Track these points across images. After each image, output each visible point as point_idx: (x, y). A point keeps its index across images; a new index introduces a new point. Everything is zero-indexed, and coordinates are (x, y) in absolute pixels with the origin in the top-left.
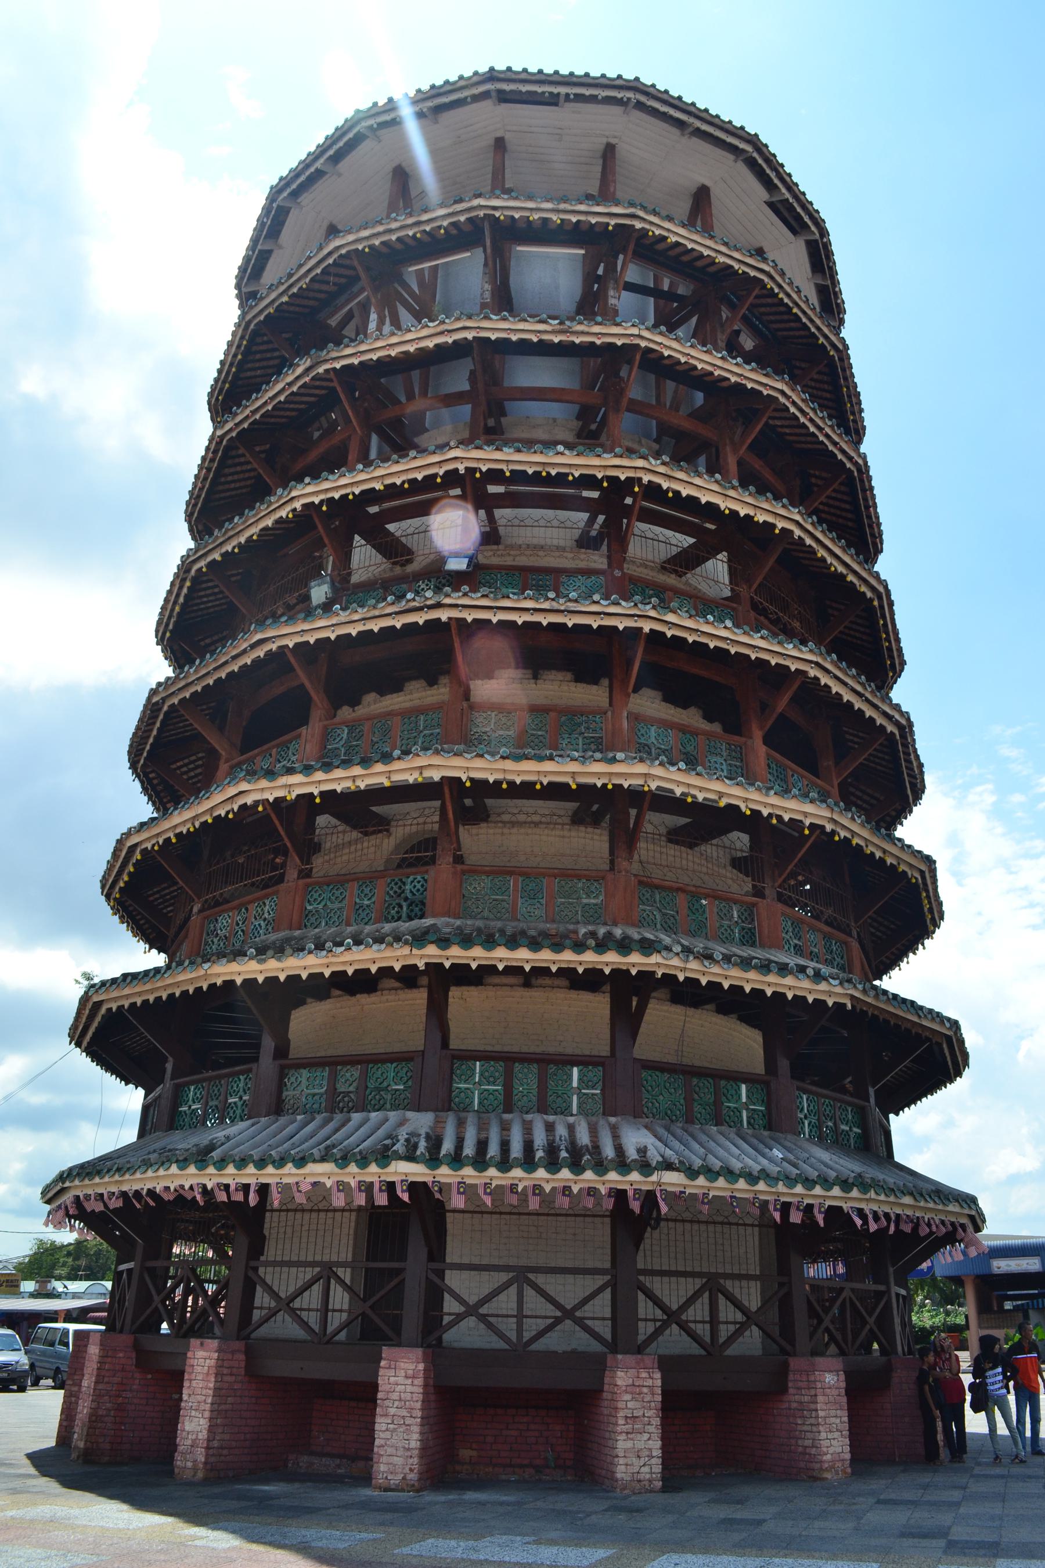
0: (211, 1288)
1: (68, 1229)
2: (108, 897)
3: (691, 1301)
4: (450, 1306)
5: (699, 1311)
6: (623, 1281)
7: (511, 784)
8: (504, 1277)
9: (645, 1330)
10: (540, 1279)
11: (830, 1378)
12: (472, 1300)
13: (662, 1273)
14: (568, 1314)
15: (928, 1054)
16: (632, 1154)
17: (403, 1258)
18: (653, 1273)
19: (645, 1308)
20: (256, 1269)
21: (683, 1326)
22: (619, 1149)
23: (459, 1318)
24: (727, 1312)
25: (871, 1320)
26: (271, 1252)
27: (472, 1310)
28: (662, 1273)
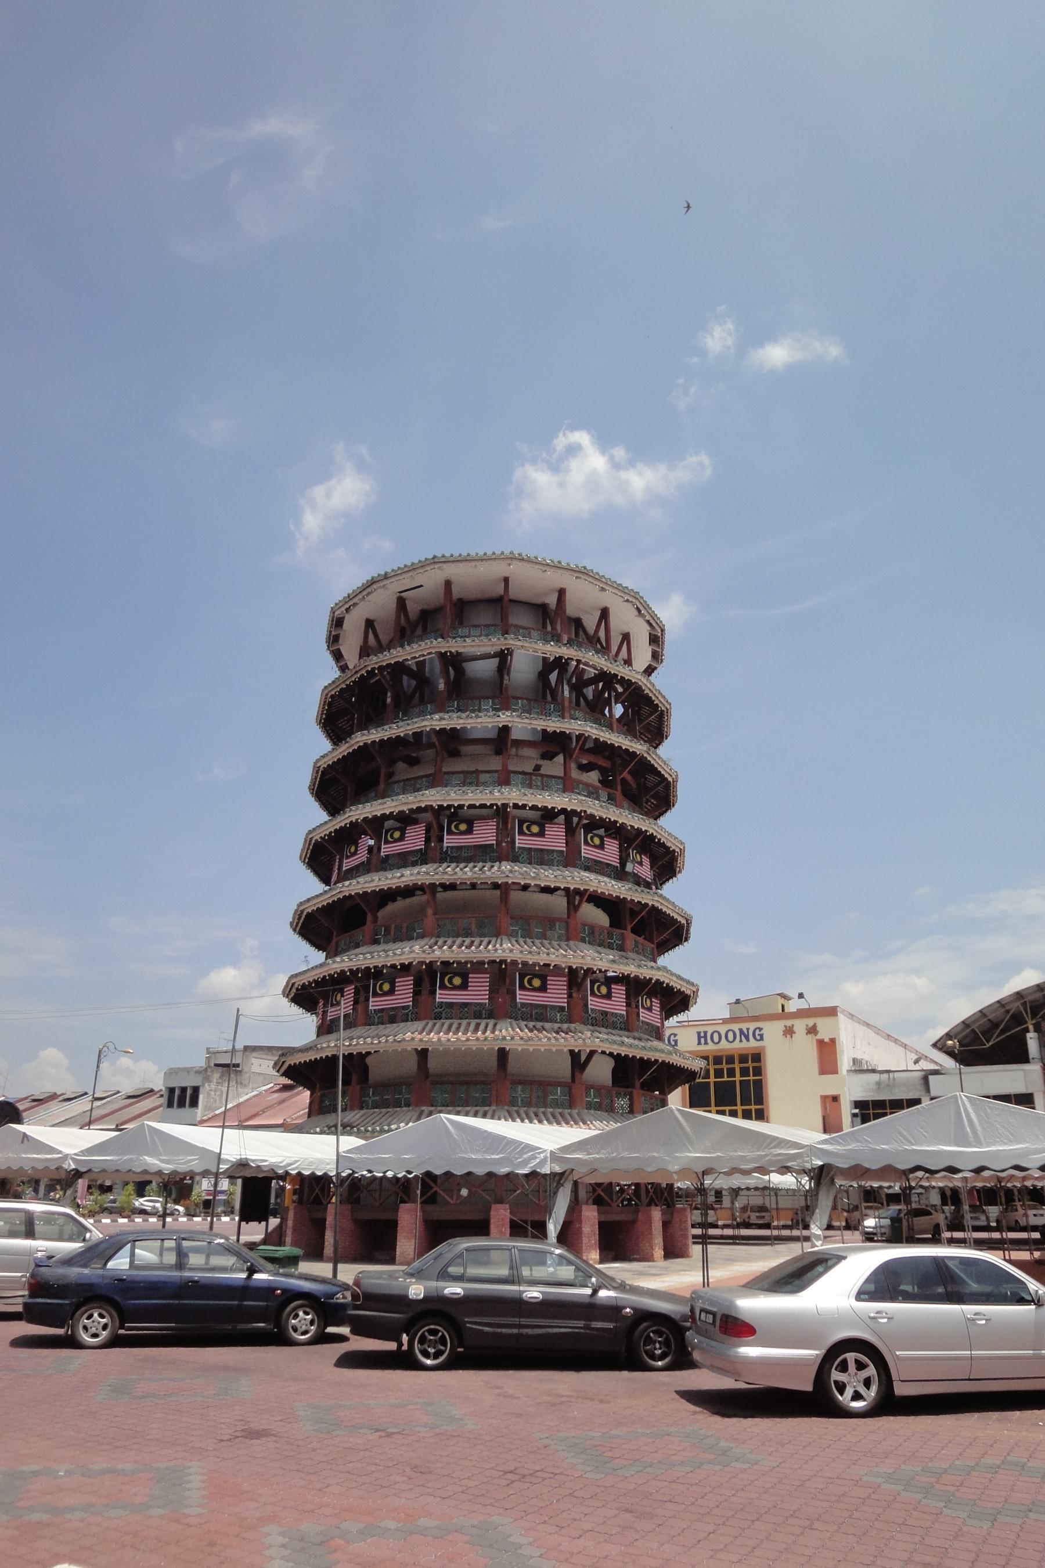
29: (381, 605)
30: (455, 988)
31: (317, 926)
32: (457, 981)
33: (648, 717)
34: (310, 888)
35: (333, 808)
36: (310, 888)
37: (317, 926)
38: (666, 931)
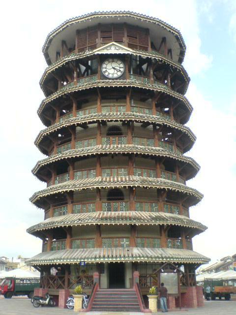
31: (44, 172)
33: (180, 81)
34: (40, 157)
35: (47, 123)
37: (44, 172)
38: (189, 170)
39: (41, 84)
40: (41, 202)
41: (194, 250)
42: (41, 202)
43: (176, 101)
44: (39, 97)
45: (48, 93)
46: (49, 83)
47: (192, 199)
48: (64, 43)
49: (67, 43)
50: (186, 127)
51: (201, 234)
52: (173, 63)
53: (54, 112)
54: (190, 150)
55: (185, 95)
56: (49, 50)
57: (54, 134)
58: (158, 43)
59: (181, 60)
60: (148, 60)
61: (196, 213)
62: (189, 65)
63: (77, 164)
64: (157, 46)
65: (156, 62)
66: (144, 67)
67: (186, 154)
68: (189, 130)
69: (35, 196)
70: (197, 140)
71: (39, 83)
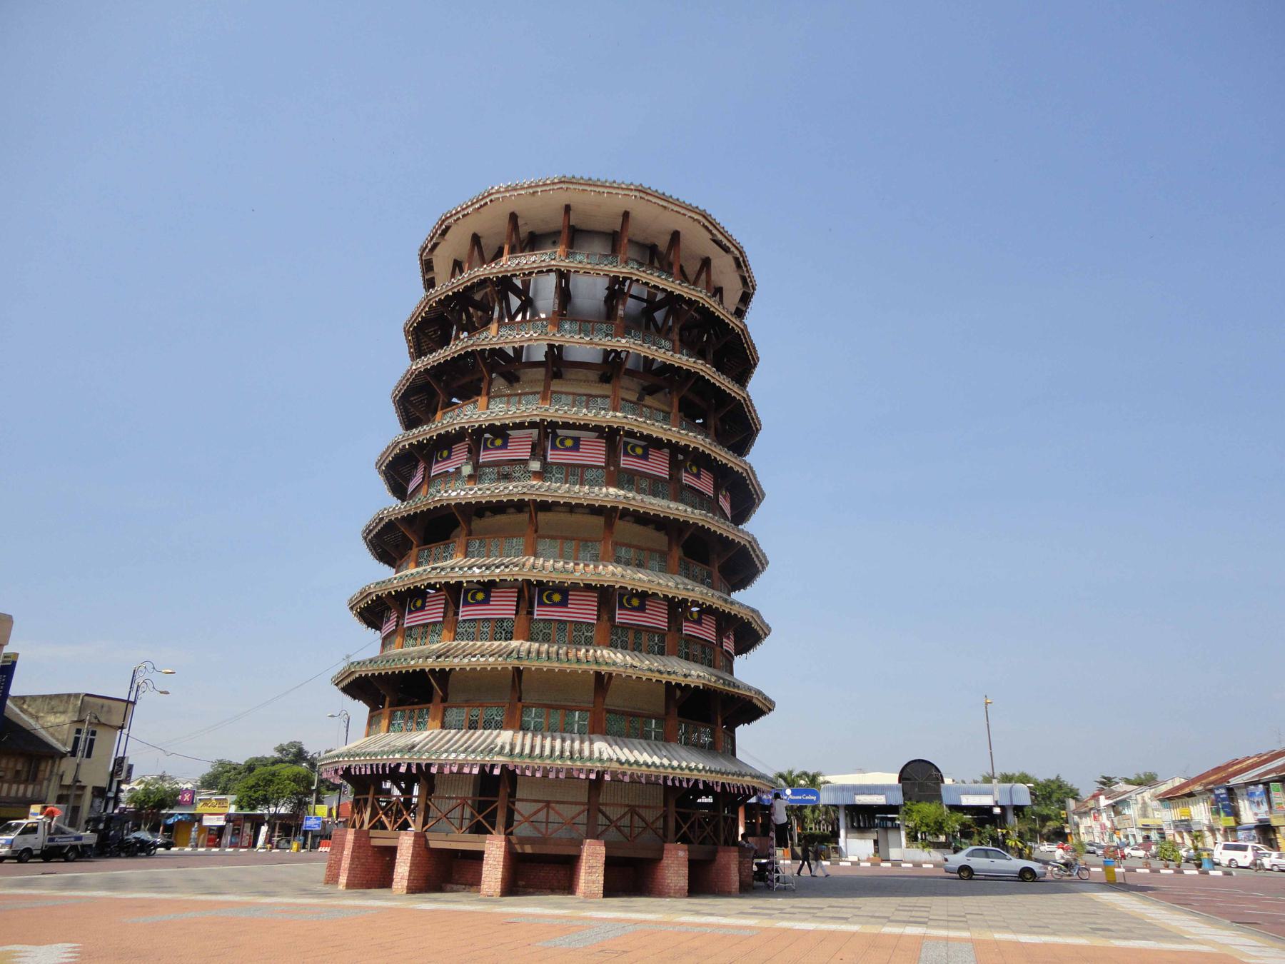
0: (1103, 802)
1: (465, 532)
2: (365, 538)
3: (623, 816)
4: (517, 817)
5: (626, 821)
6: (593, 808)
7: (642, 434)
8: (541, 805)
9: (600, 829)
10: (557, 807)
11: (681, 854)
12: (526, 814)
13: (645, 807)
14: (547, 822)
15: (749, 708)
16: (596, 755)
17: (497, 796)
18: (606, 805)
19: (601, 820)
20: (514, 803)
21: (618, 828)
22: (591, 752)
23: (521, 823)
24: (638, 822)
25: (685, 828)
26: (437, 792)
27: (527, 819)
28: (645, 807)
29: (492, 224)
30: (555, 605)
32: (480, 596)
35: (410, 422)
36: (382, 502)
37: (389, 542)
39: (407, 332)
40: (373, 611)
41: (738, 756)
42: (373, 611)
43: (726, 543)
44: (399, 364)
45: (418, 351)
46: (428, 330)
47: (747, 634)
48: (476, 239)
49: (483, 242)
50: (742, 531)
51: (762, 719)
52: (723, 311)
53: (432, 395)
54: (754, 724)
55: (748, 458)
56: (437, 251)
57: (437, 371)
58: (692, 268)
59: (740, 313)
60: (672, 300)
61: (749, 671)
62: (759, 325)
63: (477, 524)
64: (692, 276)
65: (683, 343)
66: (659, 315)
67: (737, 596)
68: (753, 542)
69: (365, 594)
70: (768, 568)
71: (402, 326)
